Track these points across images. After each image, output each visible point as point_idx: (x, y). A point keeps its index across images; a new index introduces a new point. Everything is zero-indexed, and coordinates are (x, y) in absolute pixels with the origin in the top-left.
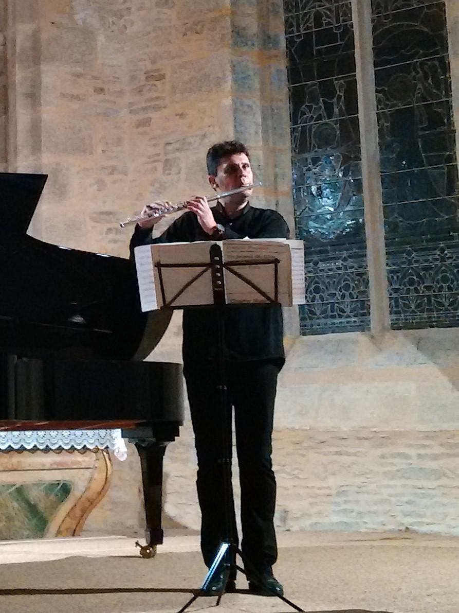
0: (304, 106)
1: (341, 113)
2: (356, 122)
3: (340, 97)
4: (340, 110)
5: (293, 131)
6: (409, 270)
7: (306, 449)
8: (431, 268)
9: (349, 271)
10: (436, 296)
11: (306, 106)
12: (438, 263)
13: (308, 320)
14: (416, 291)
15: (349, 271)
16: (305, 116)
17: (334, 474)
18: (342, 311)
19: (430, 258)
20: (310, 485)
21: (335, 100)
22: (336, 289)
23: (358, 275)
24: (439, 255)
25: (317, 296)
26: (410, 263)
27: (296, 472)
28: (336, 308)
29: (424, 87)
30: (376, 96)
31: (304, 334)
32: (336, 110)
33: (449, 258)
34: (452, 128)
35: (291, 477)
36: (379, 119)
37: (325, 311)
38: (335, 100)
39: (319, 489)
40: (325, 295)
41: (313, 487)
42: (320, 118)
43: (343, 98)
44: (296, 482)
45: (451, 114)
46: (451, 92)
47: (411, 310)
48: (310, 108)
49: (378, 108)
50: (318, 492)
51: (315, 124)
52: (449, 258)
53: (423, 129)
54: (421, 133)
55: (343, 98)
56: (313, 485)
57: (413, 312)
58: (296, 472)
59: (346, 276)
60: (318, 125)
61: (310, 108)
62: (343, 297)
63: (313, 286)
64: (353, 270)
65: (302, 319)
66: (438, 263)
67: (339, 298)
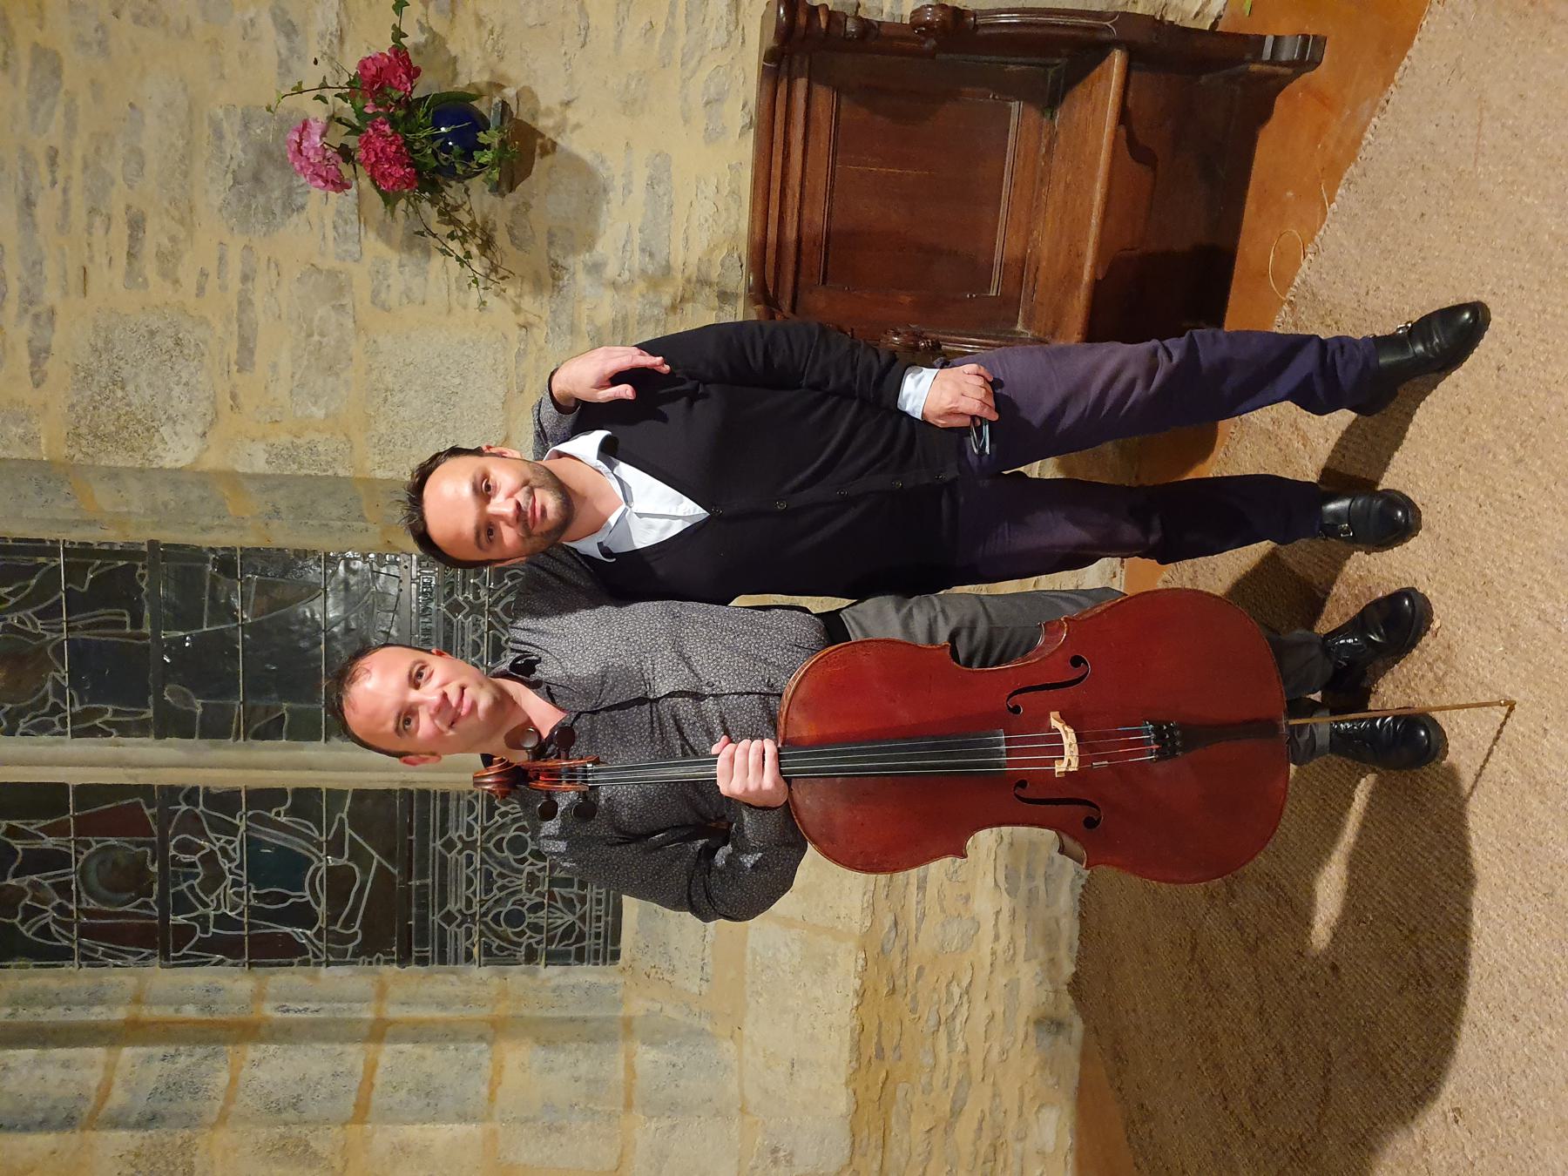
0: (23, 929)
1: (59, 830)
2: (88, 793)
3: (12, 832)
4: (49, 831)
5: (88, 959)
6: (486, 924)
7: (906, 962)
8: (489, 874)
9: (477, 835)
10: (550, 941)
11: (23, 922)
12: (484, 621)
13: (585, 943)
14: (536, 908)
15: (477, 835)
16: (53, 928)
17: (967, 898)
18: (567, 933)
19: (471, 637)
20: (988, 961)
21: (18, 846)
22: (520, 872)
23: (488, 891)
24: (466, 617)
25: (530, 918)
26: (470, 845)
27: (956, 991)
28: (560, 947)
29: (17, 607)
30: (23, 734)
31: (616, 956)
32: (50, 842)
33: (477, 597)
34: (145, 548)
35: (966, 1006)
36: (92, 732)
37: (569, 904)
38: (18, 846)
39: (997, 938)
40: (531, 899)
41: (993, 953)
42: (63, 889)
43: (14, 823)
44: (978, 997)
45: (106, 547)
46: (42, 541)
47: (578, 924)
48: (30, 912)
49: (60, 734)
50: (1004, 940)
51: (79, 901)
52: (477, 597)
53: (137, 622)
54: (147, 629)
55: (14, 823)
56: (988, 951)
57: (582, 918)
58: (956, 991)
59: (490, 845)
60: (83, 895)
61: (30, 912)
62: (538, 855)
63: (507, 853)
64: (478, 828)
65: (580, 957)
66: (476, 929)
67: (538, 937)
